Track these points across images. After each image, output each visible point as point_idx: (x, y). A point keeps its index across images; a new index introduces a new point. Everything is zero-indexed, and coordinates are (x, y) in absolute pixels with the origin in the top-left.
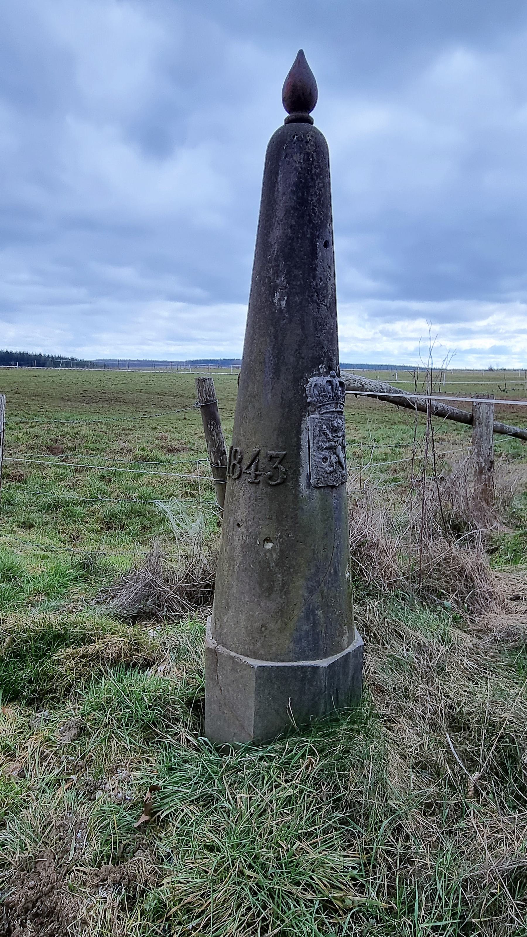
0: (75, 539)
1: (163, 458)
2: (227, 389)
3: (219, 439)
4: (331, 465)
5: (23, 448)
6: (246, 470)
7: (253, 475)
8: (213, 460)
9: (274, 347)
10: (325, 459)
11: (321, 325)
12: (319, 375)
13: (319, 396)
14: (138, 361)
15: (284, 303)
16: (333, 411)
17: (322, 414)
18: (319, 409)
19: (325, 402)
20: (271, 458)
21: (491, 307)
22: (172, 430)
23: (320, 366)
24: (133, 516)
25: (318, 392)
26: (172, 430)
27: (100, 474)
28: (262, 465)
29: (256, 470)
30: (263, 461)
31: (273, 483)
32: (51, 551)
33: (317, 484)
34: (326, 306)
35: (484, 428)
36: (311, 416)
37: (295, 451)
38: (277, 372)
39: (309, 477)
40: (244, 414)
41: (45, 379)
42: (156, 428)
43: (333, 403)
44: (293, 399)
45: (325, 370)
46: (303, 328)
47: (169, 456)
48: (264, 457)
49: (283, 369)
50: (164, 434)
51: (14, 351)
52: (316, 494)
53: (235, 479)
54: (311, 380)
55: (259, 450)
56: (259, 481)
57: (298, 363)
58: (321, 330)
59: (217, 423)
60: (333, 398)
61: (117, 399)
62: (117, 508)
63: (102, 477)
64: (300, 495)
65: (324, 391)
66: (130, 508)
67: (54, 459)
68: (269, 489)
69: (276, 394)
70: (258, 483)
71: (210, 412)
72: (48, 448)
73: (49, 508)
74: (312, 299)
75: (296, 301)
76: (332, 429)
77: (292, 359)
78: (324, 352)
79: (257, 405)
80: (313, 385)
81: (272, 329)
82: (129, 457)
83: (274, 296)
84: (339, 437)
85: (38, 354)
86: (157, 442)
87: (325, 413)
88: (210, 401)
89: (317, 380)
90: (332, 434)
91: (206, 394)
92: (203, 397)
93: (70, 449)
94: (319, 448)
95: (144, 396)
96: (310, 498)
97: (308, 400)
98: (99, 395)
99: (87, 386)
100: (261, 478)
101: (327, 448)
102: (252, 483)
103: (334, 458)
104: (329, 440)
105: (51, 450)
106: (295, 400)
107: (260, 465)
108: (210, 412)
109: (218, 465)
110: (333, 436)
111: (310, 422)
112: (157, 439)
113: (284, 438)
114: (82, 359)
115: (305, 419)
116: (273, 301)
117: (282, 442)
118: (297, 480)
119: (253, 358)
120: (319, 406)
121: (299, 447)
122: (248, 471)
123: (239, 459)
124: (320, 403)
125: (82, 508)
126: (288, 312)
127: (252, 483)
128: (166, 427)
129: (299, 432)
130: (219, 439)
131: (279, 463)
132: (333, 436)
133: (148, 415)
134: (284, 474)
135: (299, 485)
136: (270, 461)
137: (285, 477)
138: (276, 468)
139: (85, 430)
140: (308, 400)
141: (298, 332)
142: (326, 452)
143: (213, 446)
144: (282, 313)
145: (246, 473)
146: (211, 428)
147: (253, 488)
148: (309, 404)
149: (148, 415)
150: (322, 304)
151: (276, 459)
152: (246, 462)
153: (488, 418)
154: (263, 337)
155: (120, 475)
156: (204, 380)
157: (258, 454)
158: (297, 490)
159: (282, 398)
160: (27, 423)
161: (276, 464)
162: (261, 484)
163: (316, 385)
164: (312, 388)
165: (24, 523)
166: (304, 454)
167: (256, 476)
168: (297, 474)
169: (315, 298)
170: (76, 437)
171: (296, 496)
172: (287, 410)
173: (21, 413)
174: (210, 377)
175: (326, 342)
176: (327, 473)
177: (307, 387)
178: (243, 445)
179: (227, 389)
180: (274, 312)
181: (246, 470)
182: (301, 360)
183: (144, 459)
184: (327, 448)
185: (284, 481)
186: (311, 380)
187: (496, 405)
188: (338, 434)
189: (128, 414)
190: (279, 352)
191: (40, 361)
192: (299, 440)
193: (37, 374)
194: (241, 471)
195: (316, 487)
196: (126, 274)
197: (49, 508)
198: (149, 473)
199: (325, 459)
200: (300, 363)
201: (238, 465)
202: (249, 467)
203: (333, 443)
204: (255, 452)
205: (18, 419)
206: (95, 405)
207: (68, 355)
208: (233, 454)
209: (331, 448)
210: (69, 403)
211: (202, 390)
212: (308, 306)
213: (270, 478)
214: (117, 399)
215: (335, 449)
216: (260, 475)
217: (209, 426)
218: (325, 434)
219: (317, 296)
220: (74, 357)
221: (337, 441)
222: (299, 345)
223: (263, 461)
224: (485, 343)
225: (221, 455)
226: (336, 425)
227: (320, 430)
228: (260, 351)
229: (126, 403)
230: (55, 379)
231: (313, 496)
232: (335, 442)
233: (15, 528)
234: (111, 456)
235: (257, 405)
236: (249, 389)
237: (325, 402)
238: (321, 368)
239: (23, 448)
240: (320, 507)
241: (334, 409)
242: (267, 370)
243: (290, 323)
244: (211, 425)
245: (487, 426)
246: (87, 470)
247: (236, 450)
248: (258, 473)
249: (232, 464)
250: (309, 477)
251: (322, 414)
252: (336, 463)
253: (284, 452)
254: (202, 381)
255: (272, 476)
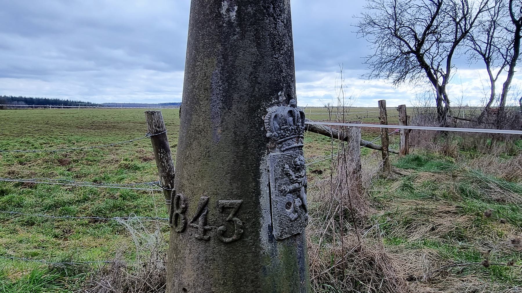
0: (66, 234)
1: (140, 165)
2: (172, 120)
3: (169, 165)
4: (295, 211)
5: (40, 162)
6: (192, 222)
7: (201, 230)
8: (164, 184)
9: (223, 69)
10: (288, 205)
11: (278, 44)
12: (278, 104)
13: (280, 129)
14: (129, 104)
15: (233, 14)
16: (295, 147)
17: (284, 151)
18: (280, 145)
19: (287, 136)
20: (224, 209)
21: (322, 74)
22: (148, 145)
23: (279, 94)
24: (115, 210)
25: (279, 125)
26: (148, 145)
27: (93, 179)
28: (212, 217)
29: (205, 223)
30: (213, 213)
31: (227, 240)
32: (43, 247)
33: (281, 236)
34: (283, 22)
35: (355, 143)
36: (272, 154)
37: (254, 198)
38: (227, 101)
39: (271, 228)
40: (188, 153)
41: (68, 115)
42: (137, 145)
43: (294, 138)
44: (249, 134)
45: (284, 98)
46: (258, 45)
47: (144, 164)
48: (215, 208)
49: (236, 96)
50: (142, 149)
51: (50, 98)
52: (280, 248)
53: (179, 232)
54: (270, 110)
55: (208, 199)
56: (210, 237)
57: (254, 89)
58: (279, 50)
59: (167, 151)
60: (295, 132)
61: (114, 127)
62: (102, 205)
63: (95, 181)
64: (262, 252)
65: (286, 123)
66: (112, 205)
67: (63, 169)
68: (223, 248)
69: (227, 129)
70: (209, 239)
71: (159, 141)
72: (59, 161)
73: (50, 208)
74: (267, 11)
75: (249, 13)
76: (295, 168)
77: (246, 84)
78: (283, 77)
79: (203, 142)
80: (273, 117)
81: (219, 46)
82: (116, 165)
83: (220, 6)
84: (303, 177)
85: (66, 100)
86: (136, 154)
87: (287, 150)
88: (160, 132)
89: (276, 110)
90: (295, 174)
91: (155, 126)
92: (153, 128)
93: (74, 161)
94: (282, 192)
95: (132, 125)
96: (273, 254)
97: (268, 135)
98: (102, 124)
99: (95, 119)
100: (211, 234)
101: (290, 192)
102: (201, 240)
103: (298, 202)
104: (293, 182)
105: (61, 162)
106: (251, 134)
107: (210, 217)
108: (159, 141)
109: (169, 188)
110: (296, 177)
111: (270, 162)
112: (137, 152)
113: (239, 183)
114: (31, 96)
115: (264, 158)
116: (219, 12)
117: (237, 188)
118: (258, 234)
119: (196, 84)
120: (279, 141)
121: (258, 193)
122: (195, 225)
123: (183, 208)
124: (281, 139)
125: (76, 207)
126: (240, 25)
127: (201, 240)
128: (143, 144)
129: (257, 175)
130: (169, 165)
131: (234, 215)
132: (296, 177)
133: (132, 136)
134: (241, 228)
135: (260, 240)
136: (222, 212)
137: (242, 231)
138: (230, 221)
139: (87, 148)
140: (268, 135)
141: (253, 50)
142: (290, 196)
143: (163, 171)
144: (232, 26)
145: (193, 227)
146: (161, 155)
147: (202, 246)
148: (268, 139)
149: (132, 136)
150: (279, 19)
151: (231, 209)
152: (192, 213)
153: (357, 136)
154: (208, 57)
155: (109, 178)
156: (153, 113)
157: (207, 203)
158: (257, 247)
159: (235, 133)
160: (49, 143)
161: (231, 216)
162: (212, 241)
163: (276, 116)
164: (272, 120)
165: (27, 222)
166: (264, 201)
167: (205, 232)
168: (257, 226)
169: (271, 10)
170: (81, 153)
171: (256, 255)
172: (242, 147)
173: (46, 137)
174: (158, 111)
175: (284, 65)
176: (291, 221)
177: (266, 118)
178: (188, 191)
179: (172, 120)
180: (222, 26)
181: (192, 222)
182: (257, 85)
183: (127, 167)
184: (290, 192)
185: (242, 237)
186: (270, 110)
187: (364, 129)
188: (301, 173)
189: (120, 136)
190: (229, 77)
191: (67, 104)
192: (258, 184)
193: (63, 112)
194: (186, 223)
195: (279, 240)
196: (119, 53)
197: (50, 208)
198: (129, 177)
199: (288, 205)
200: (257, 90)
201: (182, 216)
202: (195, 220)
203: (297, 185)
204: (202, 202)
205: (42, 141)
206: (99, 131)
207: (86, 101)
208: (175, 202)
209: (296, 192)
210: (82, 130)
211: (152, 122)
212: (263, 20)
213: (224, 234)
214: (114, 127)
215: (299, 191)
216: (210, 230)
217: (159, 154)
218: (288, 175)
219: (274, 8)
220: (89, 102)
221: (301, 182)
222: (254, 67)
223: (213, 213)
224: (321, 93)
225: (171, 179)
226: (299, 163)
227: (283, 170)
228: (205, 75)
229: (120, 129)
230: (74, 115)
231: (276, 251)
232: (299, 183)
233: (18, 227)
234: (104, 165)
235: (203, 142)
236: (193, 123)
237: (287, 136)
238: (281, 95)
239: (40, 162)
240: (284, 263)
241: (296, 145)
242: (214, 98)
243: (242, 39)
244: (161, 153)
245: (357, 142)
246: (85, 177)
247: (179, 197)
248: (207, 227)
249: (174, 213)
250: (271, 228)
251: (284, 151)
252: (300, 207)
253: (240, 201)
254: (150, 114)
255: (225, 231)
